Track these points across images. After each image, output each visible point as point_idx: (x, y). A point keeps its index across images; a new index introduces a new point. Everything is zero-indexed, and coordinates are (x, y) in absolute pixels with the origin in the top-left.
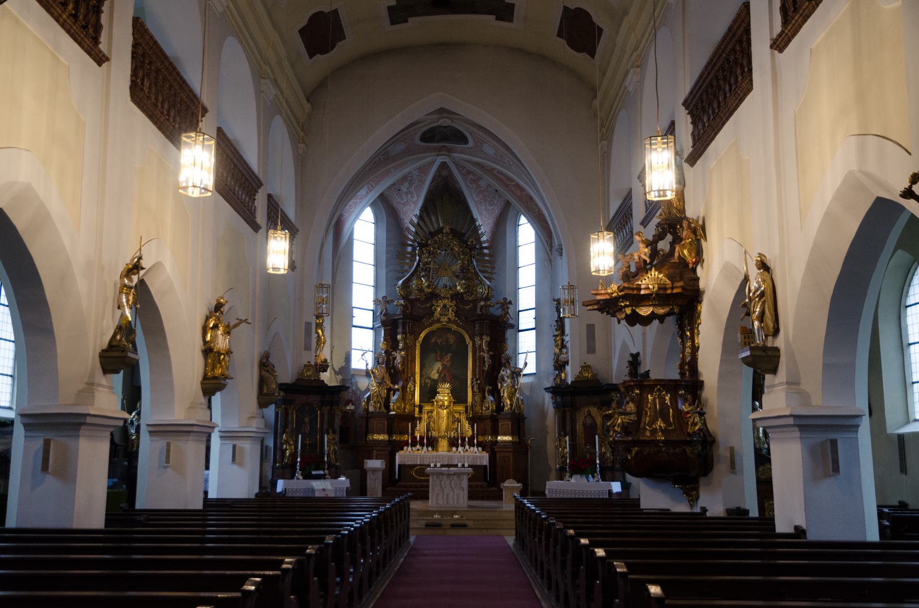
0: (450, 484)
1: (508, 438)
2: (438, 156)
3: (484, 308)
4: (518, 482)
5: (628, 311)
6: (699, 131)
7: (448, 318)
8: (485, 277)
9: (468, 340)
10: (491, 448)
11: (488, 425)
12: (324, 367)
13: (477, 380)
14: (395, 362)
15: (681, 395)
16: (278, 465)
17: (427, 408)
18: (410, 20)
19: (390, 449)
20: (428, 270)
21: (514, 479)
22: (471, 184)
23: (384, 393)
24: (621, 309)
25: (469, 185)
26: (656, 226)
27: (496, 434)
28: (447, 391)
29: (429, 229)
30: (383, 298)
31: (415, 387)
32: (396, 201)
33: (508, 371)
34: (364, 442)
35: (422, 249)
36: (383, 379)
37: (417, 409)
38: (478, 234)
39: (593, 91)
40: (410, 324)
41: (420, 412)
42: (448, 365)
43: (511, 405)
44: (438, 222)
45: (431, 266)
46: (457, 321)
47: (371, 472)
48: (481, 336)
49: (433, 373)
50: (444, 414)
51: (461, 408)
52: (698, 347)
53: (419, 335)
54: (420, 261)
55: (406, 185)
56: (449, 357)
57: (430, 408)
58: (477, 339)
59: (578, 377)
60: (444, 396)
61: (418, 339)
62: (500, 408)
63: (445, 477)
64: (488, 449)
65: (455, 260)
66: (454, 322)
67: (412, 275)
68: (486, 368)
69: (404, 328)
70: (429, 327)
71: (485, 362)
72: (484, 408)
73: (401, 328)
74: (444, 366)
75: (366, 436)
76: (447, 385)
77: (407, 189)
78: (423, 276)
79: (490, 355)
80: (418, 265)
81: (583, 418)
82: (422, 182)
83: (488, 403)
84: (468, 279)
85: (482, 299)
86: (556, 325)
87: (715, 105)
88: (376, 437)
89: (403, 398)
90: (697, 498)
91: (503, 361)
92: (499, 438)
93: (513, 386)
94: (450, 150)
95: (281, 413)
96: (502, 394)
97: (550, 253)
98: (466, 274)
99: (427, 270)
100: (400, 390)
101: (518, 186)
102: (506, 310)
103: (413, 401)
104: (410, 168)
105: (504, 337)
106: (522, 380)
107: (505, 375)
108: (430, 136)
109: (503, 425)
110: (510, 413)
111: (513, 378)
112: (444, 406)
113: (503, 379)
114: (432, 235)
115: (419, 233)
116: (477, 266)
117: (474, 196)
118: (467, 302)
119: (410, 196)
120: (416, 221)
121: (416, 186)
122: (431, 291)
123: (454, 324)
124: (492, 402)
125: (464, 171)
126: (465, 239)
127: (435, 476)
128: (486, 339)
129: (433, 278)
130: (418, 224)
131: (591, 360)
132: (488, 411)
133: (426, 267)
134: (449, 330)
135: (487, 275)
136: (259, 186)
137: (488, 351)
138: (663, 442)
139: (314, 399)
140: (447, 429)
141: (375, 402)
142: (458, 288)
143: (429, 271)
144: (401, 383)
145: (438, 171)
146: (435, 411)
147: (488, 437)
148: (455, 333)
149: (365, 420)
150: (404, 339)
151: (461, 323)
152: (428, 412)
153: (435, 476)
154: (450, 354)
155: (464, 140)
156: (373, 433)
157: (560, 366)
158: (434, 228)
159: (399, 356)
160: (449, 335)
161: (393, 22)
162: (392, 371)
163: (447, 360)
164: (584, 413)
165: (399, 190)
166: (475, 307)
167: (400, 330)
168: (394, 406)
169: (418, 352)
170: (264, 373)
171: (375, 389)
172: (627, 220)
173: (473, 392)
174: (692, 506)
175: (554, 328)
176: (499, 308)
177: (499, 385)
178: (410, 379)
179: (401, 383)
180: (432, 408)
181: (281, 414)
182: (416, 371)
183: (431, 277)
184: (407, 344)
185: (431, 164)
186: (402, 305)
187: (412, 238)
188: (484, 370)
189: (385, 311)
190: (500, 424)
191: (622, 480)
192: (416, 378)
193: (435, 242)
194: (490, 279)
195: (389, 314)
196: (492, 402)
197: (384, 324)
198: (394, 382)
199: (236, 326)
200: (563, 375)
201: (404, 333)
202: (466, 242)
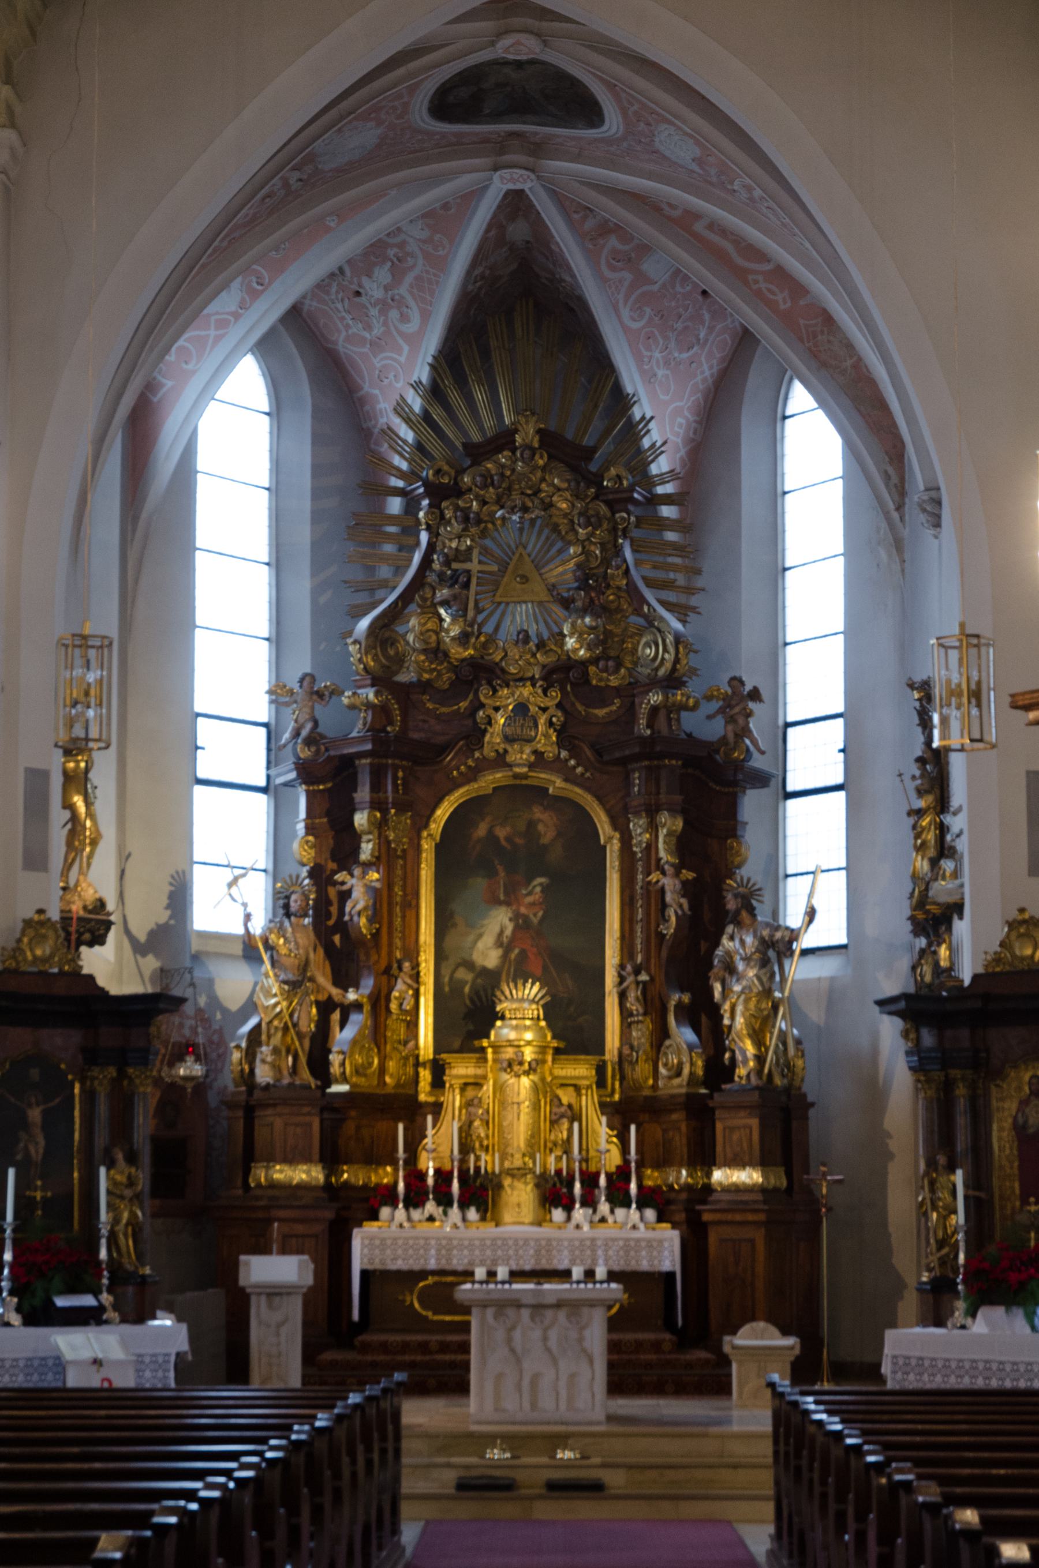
0: (545, 1339)
13: (637, 972)
14: (347, 909)
17: (461, 1069)
19: (329, 1215)
20: (463, 579)
34: (240, 1192)
35: (439, 507)
37: (425, 1076)
40: (400, 774)
45: (474, 566)
46: (567, 760)
55: (383, 274)
56: (538, 889)
63: (525, 1313)
64: (681, 1217)
68: (670, 928)
69: (377, 786)
72: (663, 1071)
79: (685, 883)
92: (718, 1175)
100: (367, 1008)
103: (411, 1044)
119: (394, 314)
124: (691, 1047)
127: (490, 1312)
132: (676, 1081)
133: (455, 571)
143: (466, 585)
144: (368, 984)
146: (491, 1082)
151: (579, 770)
152: (466, 1084)
153: (490, 1312)
162: (337, 939)
179: (368, 984)
180: (480, 1072)
183: (471, 605)
184: (388, 843)
188: (661, 936)
190: (719, 1126)
192: (423, 965)
196: (691, 1047)
201: (378, 805)
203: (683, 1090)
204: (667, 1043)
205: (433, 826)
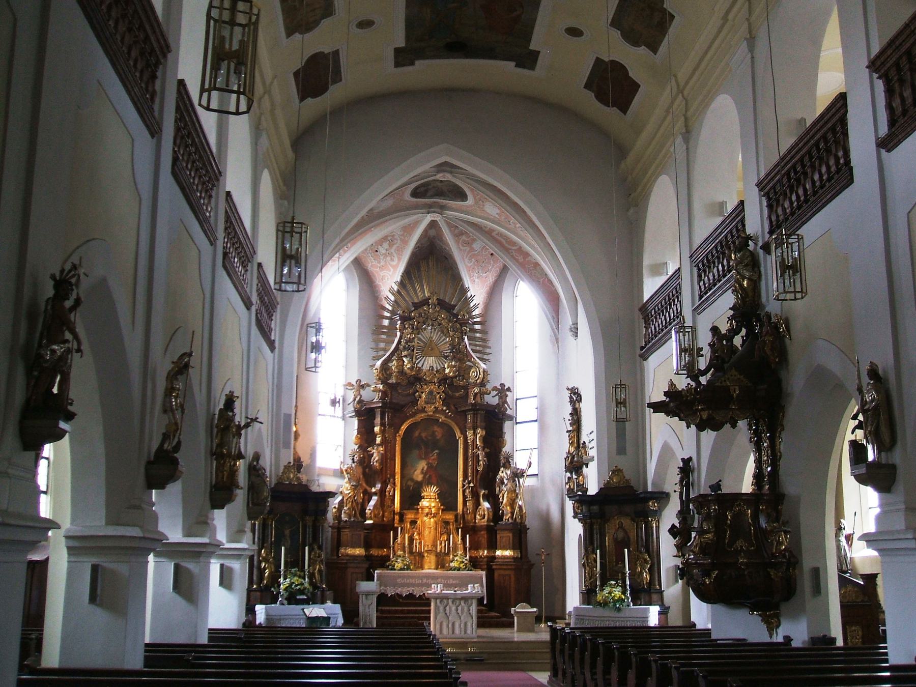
0: (457, 610)
1: (508, 553)
2: (428, 213)
3: (479, 394)
8: (478, 358)
9: (458, 434)
10: (490, 566)
11: (483, 537)
13: (469, 483)
15: (762, 510)
16: (255, 587)
17: (410, 516)
18: (417, 62)
22: (463, 246)
25: (462, 248)
26: (728, 318)
27: (493, 546)
30: (357, 381)
32: (372, 265)
34: (336, 557)
36: (359, 482)
37: (397, 517)
39: (622, 151)
41: (402, 520)
45: (415, 344)
47: (364, 596)
49: (416, 473)
50: (432, 524)
51: (450, 517)
53: (401, 427)
54: (401, 337)
55: (386, 245)
57: (413, 516)
60: (429, 501)
61: (398, 432)
62: (496, 515)
63: (450, 601)
65: (444, 337)
66: (443, 412)
67: (393, 354)
68: (480, 469)
69: (382, 418)
70: (412, 417)
71: (479, 461)
72: (478, 517)
73: (379, 419)
74: (430, 466)
75: (338, 550)
76: (434, 489)
77: (387, 250)
78: (405, 356)
80: (399, 342)
81: (613, 531)
82: (405, 242)
83: (484, 511)
84: (460, 360)
85: (475, 385)
86: (571, 418)
88: (350, 551)
91: (503, 461)
92: (499, 553)
94: (443, 208)
95: (259, 525)
96: (501, 500)
97: (556, 330)
101: (520, 250)
102: (504, 398)
104: (393, 227)
105: (502, 430)
107: (504, 477)
109: (503, 537)
110: (511, 523)
112: (431, 514)
113: (502, 483)
114: (417, 306)
115: (400, 303)
117: (466, 260)
118: (458, 388)
119: (388, 258)
120: (396, 288)
121: (398, 247)
122: (414, 375)
123: (443, 414)
124: (488, 508)
125: (457, 231)
126: (455, 312)
130: (398, 292)
131: (624, 463)
132: (483, 520)
135: (478, 355)
138: (746, 564)
142: (447, 371)
144: (379, 486)
145: (426, 231)
147: (484, 552)
148: (443, 425)
149: (336, 530)
150: (383, 432)
154: (437, 451)
155: (463, 196)
156: (347, 546)
158: (418, 298)
159: (376, 454)
160: (436, 428)
161: (397, 64)
163: (433, 458)
164: (616, 526)
165: (377, 251)
166: (467, 395)
167: (378, 420)
169: (398, 448)
171: (349, 493)
173: (464, 497)
175: (568, 423)
176: (496, 395)
177: (497, 489)
178: (389, 481)
182: (396, 471)
185: (417, 223)
186: (380, 391)
187: (390, 308)
188: (477, 471)
189: (359, 397)
190: (498, 536)
191: (660, 603)
195: (364, 401)
199: (247, 425)
202: (456, 316)
203: (486, 524)
204: (480, 507)
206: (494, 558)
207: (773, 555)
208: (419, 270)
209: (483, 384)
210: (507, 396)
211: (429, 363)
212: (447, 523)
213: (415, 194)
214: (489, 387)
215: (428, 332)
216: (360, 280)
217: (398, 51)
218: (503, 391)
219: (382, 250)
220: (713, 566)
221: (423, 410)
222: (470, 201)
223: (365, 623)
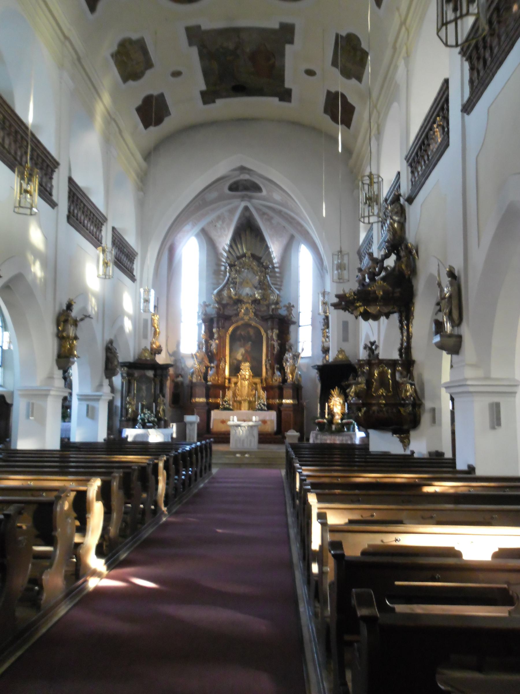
4: (297, 432)
5: (362, 309)
6: (415, 178)
7: (249, 317)
8: (276, 288)
9: (263, 333)
10: (279, 409)
12: (159, 351)
15: (399, 371)
17: (234, 380)
21: (294, 429)
23: (203, 370)
24: (357, 308)
27: (281, 397)
28: (248, 368)
29: (236, 253)
31: (225, 365)
32: (214, 234)
33: (291, 354)
37: (227, 381)
38: (271, 257)
41: (230, 382)
42: (249, 350)
43: (293, 378)
44: (243, 249)
48: (272, 329)
51: (257, 380)
52: (412, 336)
54: (229, 276)
58: (269, 332)
59: (336, 358)
60: (246, 371)
62: (284, 381)
67: (224, 287)
69: (218, 323)
72: (273, 380)
74: (246, 351)
75: (191, 399)
80: (228, 279)
85: (273, 304)
87: (426, 158)
89: (217, 373)
90: (409, 444)
92: (284, 401)
93: (294, 365)
98: (263, 286)
99: (235, 283)
100: (215, 367)
106: (300, 361)
108: (234, 187)
111: (294, 359)
112: (245, 378)
113: (287, 360)
114: (238, 258)
116: (270, 280)
120: (227, 248)
128: (276, 331)
129: (238, 289)
130: (229, 252)
131: (347, 347)
134: (250, 325)
135: (277, 287)
136: (105, 220)
137: (277, 341)
138: (384, 404)
139: (150, 374)
140: (248, 395)
141: (197, 376)
142: (257, 295)
143: (236, 284)
144: (216, 362)
150: (218, 332)
157: (326, 351)
159: (214, 344)
167: (215, 325)
168: (210, 379)
170: (109, 354)
172: (370, 246)
173: (266, 369)
174: (405, 450)
175: (322, 324)
177: (284, 364)
179: (216, 362)
181: (125, 383)
185: (236, 208)
186: (216, 308)
188: (273, 354)
193: (241, 263)
194: (279, 290)
196: (279, 376)
197: (204, 321)
198: (211, 361)
199: (82, 320)
200: (327, 357)
201: (218, 327)
205: (229, 331)
206: (281, 404)
207: (403, 399)
208: (241, 238)
209: (277, 303)
210: (292, 310)
211: (247, 290)
212: (256, 384)
213: (231, 189)
214: (282, 304)
215: (245, 272)
216: (207, 243)
217: (203, 93)
218: (290, 307)
219: (219, 225)
220: (364, 405)
221: (242, 319)
222: (264, 193)
223: (190, 439)
